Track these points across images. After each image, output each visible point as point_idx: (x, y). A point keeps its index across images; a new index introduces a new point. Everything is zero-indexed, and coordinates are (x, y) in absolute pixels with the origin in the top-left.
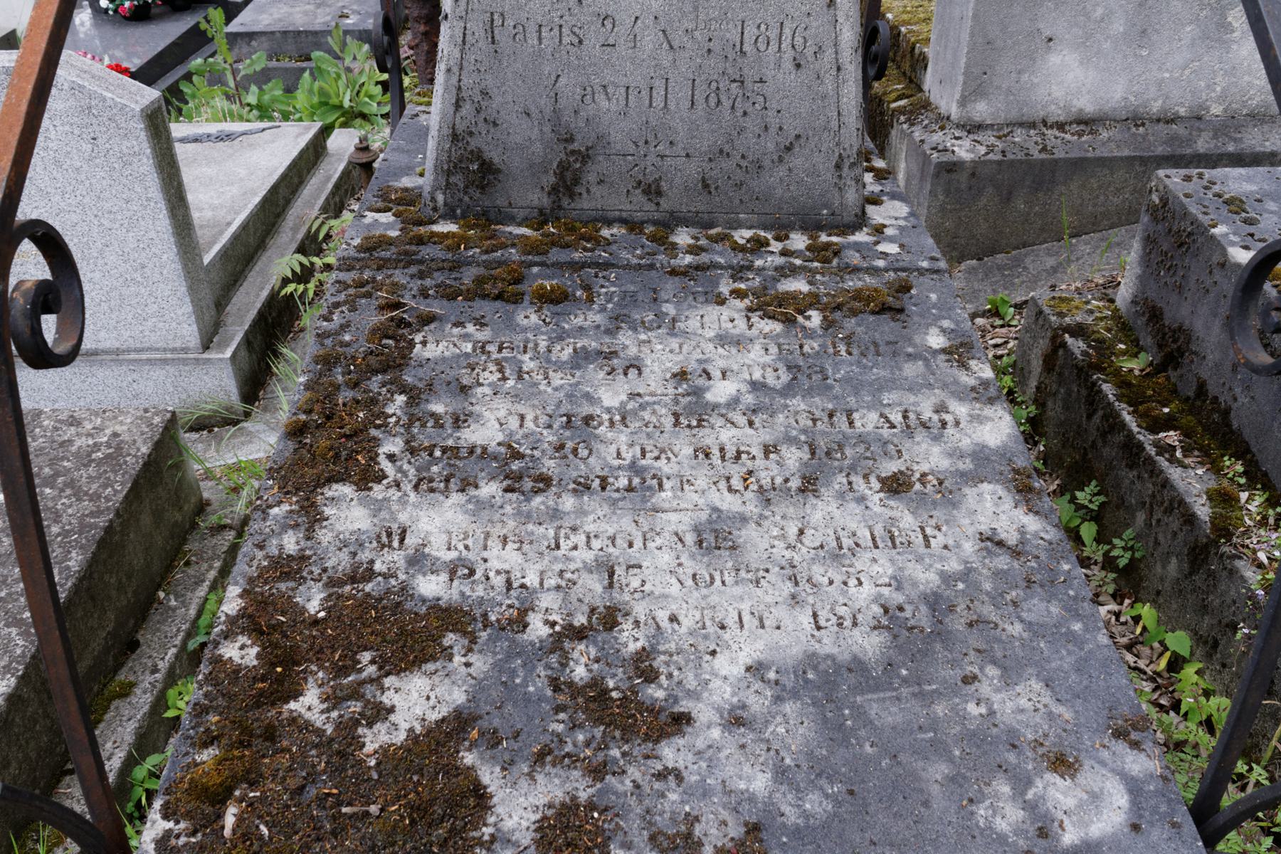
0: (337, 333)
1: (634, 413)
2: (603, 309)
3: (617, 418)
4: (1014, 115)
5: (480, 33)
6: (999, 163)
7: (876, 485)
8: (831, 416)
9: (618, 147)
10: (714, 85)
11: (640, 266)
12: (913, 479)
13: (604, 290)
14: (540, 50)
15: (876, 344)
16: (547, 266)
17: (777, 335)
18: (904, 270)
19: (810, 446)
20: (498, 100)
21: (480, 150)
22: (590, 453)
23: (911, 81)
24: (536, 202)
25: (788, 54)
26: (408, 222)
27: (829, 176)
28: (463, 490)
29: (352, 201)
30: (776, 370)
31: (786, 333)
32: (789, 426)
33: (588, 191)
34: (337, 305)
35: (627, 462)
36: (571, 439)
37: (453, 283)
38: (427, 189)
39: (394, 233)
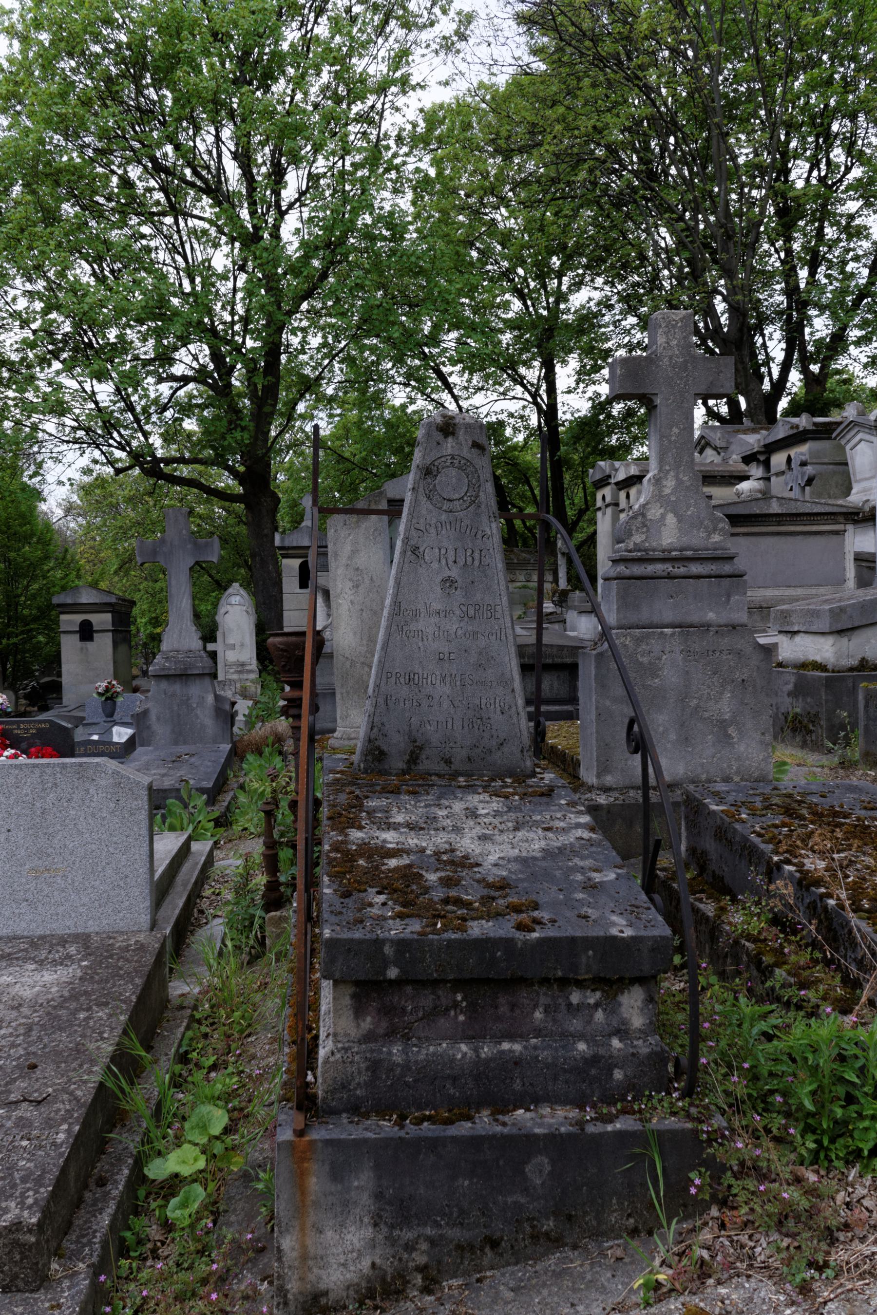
27: (519, 755)
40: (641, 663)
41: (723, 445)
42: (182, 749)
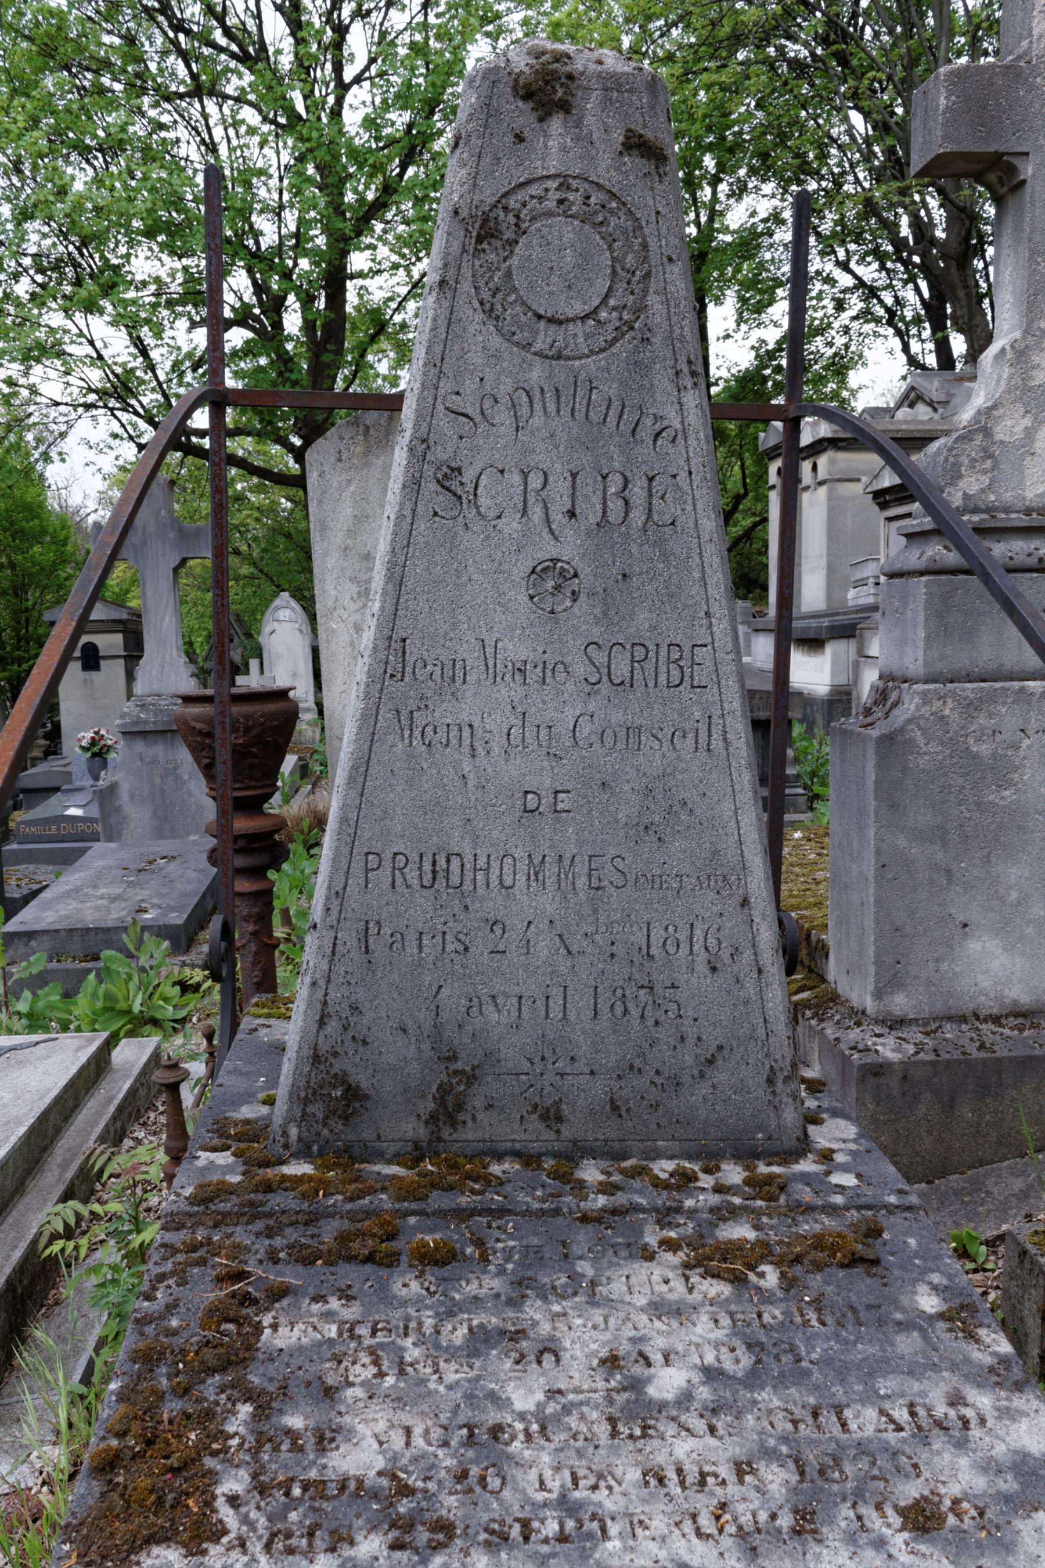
0: (162, 1317)
1: (557, 1418)
2: (501, 1272)
3: (535, 1427)
4: (939, 1008)
5: (352, 942)
6: (934, 1064)
7: (896, 1521)
8: (815, 1415)
9: (510, 1065)
10: (619, 992)
11: (542, 1212)
12: (944, 1509)
13: (500, 1245)
14: (421, 959)
15: (854, 1310)
16: (428, 1215)
17: (727, 1300)
18: (869, 1207)
19: (796, 1461)
20: (369, 1015)
21: (345, 1073)
22: (503, 1484)
23: (811, 971)
24: (410, 1134)
25: (702, 957)
26: (252, 1163)
27: (761, 1092)
28: (332, 1549)
29: (136, 1127)
30: (733, 1350)
31: (738, 1297)
32: (762, 1432)
33: (474, 1118)
34: (162, 1277)
35: (554, 1496)
36: (476, 1461)
37: (310, 1242)
38: (278, 1121)
39: (235, 1179)
40: (975, 756)
41: (942, 398)
42: (165, 846)
